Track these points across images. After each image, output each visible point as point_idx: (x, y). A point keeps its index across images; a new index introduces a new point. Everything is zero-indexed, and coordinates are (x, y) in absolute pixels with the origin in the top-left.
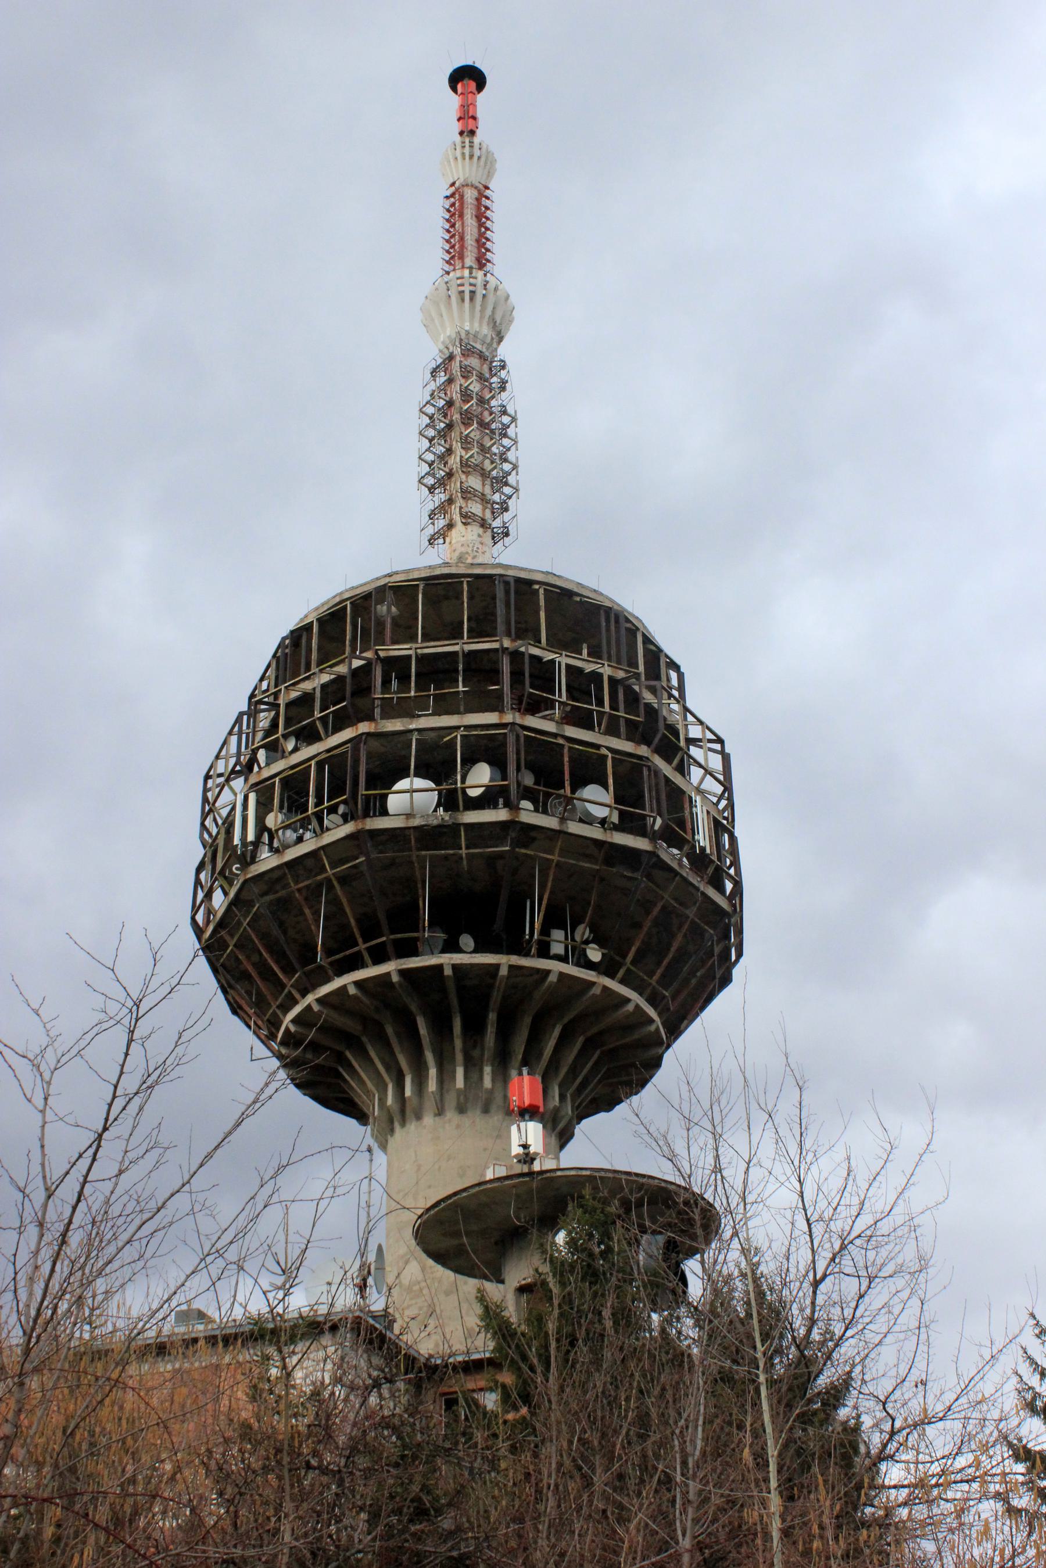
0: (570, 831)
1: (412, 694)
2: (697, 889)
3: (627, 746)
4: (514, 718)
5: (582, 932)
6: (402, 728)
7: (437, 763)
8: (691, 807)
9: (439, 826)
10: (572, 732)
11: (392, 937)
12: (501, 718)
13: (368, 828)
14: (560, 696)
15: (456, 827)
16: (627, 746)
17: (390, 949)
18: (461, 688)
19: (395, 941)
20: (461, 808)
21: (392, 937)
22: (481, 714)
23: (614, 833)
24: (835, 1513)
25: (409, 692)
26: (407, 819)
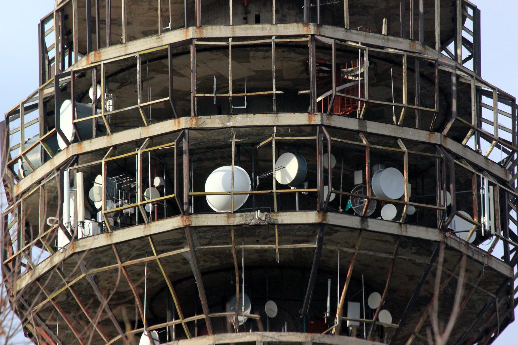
0: (370, 228)
1: (230, 94)
2: (482, 264)
3: (420, 135)
4: (322, 120)
5: (375, 300)
6: (221, 126)
7: (254, 156)
8: (479, 191)
9: (256, 226)
10: (373, 127)
11: (211, 315)
12: (310, 119)
13: (193, 224)
14: (362, 95)
15: (272, 225)
16: (420, 135)
17: (208, 324)
18: (274, 91)
19: (212, 319)
20: (276, 210)
21: (211, 315)
22: (292, 115)
23: (408, 226)
24: (68, 301)
25: (227, 92)
26: (228, 217)
